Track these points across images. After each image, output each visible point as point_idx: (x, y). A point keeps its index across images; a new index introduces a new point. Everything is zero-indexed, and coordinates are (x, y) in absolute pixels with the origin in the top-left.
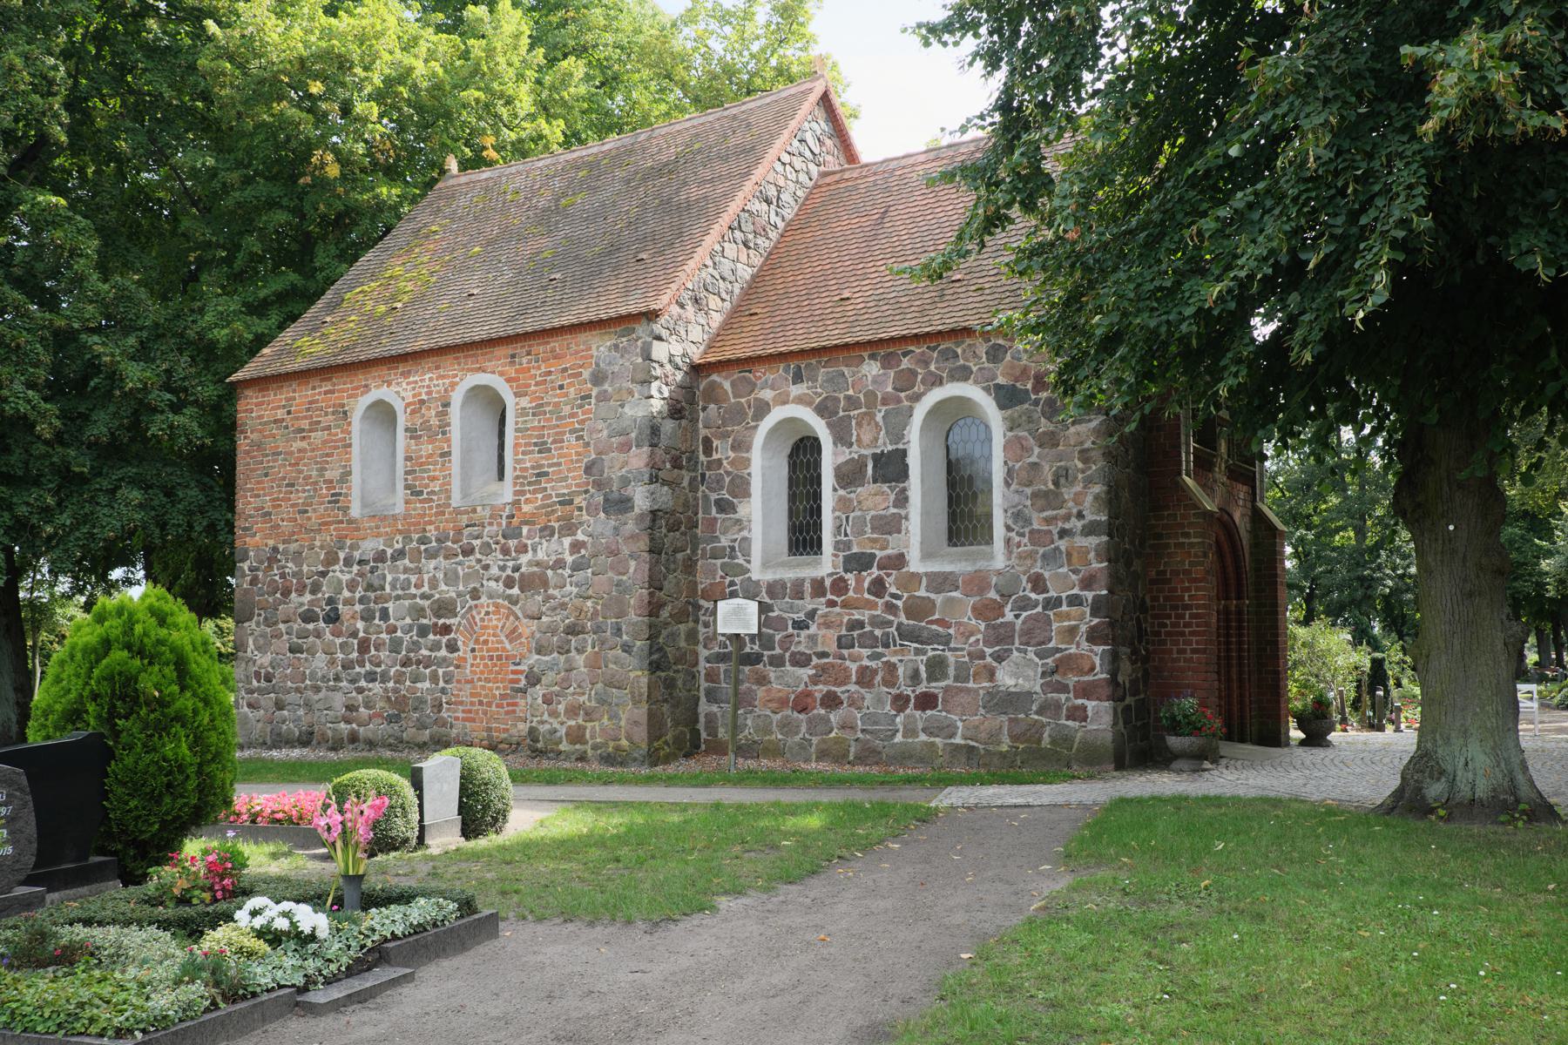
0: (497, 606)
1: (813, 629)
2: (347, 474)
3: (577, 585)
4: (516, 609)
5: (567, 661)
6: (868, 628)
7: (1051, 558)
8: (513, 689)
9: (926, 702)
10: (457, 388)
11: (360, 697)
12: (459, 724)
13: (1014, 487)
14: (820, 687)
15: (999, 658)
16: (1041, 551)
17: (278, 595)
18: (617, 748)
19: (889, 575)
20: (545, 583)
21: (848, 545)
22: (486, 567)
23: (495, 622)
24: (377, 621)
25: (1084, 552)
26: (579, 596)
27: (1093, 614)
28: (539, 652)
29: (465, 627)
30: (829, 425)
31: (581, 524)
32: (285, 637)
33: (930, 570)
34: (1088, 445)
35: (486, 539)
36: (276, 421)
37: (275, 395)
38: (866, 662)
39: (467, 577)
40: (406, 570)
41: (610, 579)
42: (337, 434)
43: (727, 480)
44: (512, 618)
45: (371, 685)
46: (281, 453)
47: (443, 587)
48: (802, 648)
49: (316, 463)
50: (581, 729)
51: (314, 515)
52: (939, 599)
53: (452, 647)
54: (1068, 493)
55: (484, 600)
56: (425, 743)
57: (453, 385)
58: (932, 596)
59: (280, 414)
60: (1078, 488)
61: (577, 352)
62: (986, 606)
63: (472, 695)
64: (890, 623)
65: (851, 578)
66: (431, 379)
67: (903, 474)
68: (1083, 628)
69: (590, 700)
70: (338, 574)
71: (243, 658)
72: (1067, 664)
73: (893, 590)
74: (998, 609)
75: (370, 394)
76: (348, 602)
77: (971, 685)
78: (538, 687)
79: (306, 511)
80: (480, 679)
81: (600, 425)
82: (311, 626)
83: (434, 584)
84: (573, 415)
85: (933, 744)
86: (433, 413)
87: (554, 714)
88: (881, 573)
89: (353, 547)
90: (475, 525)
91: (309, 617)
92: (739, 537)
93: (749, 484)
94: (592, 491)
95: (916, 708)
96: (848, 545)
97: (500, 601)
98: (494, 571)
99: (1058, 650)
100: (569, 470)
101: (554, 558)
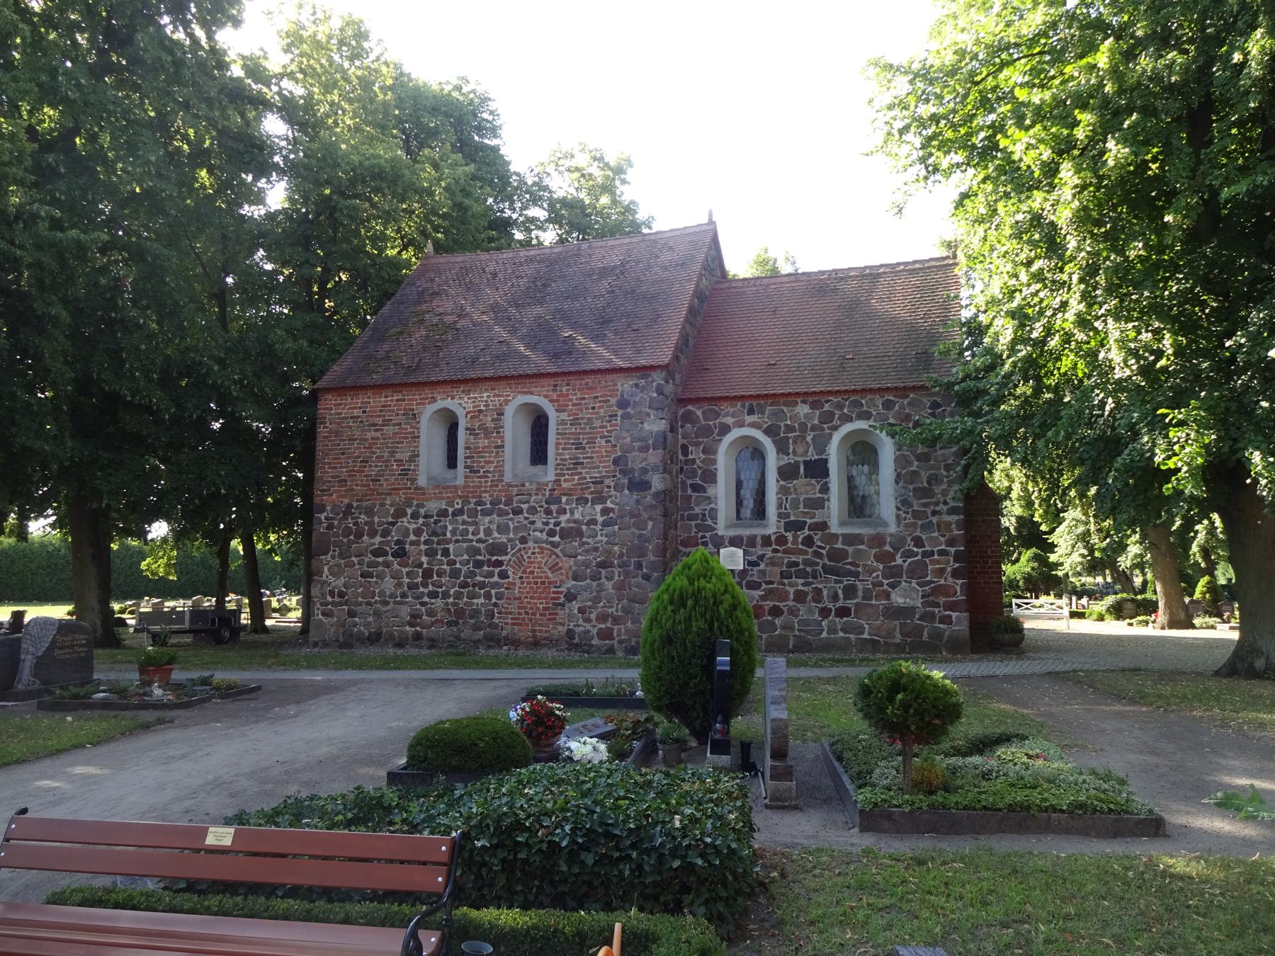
1: (762, 566)
2: (414, 457)
3: (606, 536)
4: (557, 551)
5: (599, 585)
7: (927, 527)
8: (553, 604)
9: (843, 612)
10: (510, 404)
11: (423, 609)
12: (509, 627)
13: (901, 485)
15: (893, 586)
16: (920, 523)
17: (352, 537)
19: (816, 534)
20: (580, 534)
21: (788, 515)
22: (533, 523)
23: (539, 559)
24: (439, 557)
27: (954, 561)
28: (575, 579)
29: (514, 562)
30: (774, 442)
31: (610, 497)
32: (357, 567)
33: (845, 532)
34: (950, 461)
35: (532, 504)
36: (352, 418)
37: (352, 399)
38: (800, 588)
39: (516, 529)
40: (464, 523)
43: (700, 472)
44: (554, 556)
45: (433, 601)
46: (356, 439)
47: (496, 535)
48: (755, 578)
49: (388, 447)
50: (610, 631)
51: (385, 484)
52: (850, 549)
53: (503, 575)
55: (530, 544)
57: (507, 402)
58: (846, 547)
59: (356, 412)
61: (606, 387)
63: (519, 608)
64: (818, 564)
65: (789, 536)
66: (488, 397)
67: (826, 473)
68: (949, 569)
69: (617, 611)
70: (405, 524)
71: (318, 581)
72: (938, 590)
73: (819, 543)
75: (554, 412)
76: (412, 543)
77: (873, 602)
79: (379, 480)
80: (526, 597)
82: (380, 560)
83: (488, 532)
84: (602, 427)
87: (588, 620)
89: (420, 506)
90: (523, 494)
91: (379, 552)
92: (708, 508)
93: (716, 475)
94: (619, 476)
95: (836, 616)
96: (788, 515)
97: (544, 545)
99: (932, 582)
100: (600, 462)
101: (588, 518)
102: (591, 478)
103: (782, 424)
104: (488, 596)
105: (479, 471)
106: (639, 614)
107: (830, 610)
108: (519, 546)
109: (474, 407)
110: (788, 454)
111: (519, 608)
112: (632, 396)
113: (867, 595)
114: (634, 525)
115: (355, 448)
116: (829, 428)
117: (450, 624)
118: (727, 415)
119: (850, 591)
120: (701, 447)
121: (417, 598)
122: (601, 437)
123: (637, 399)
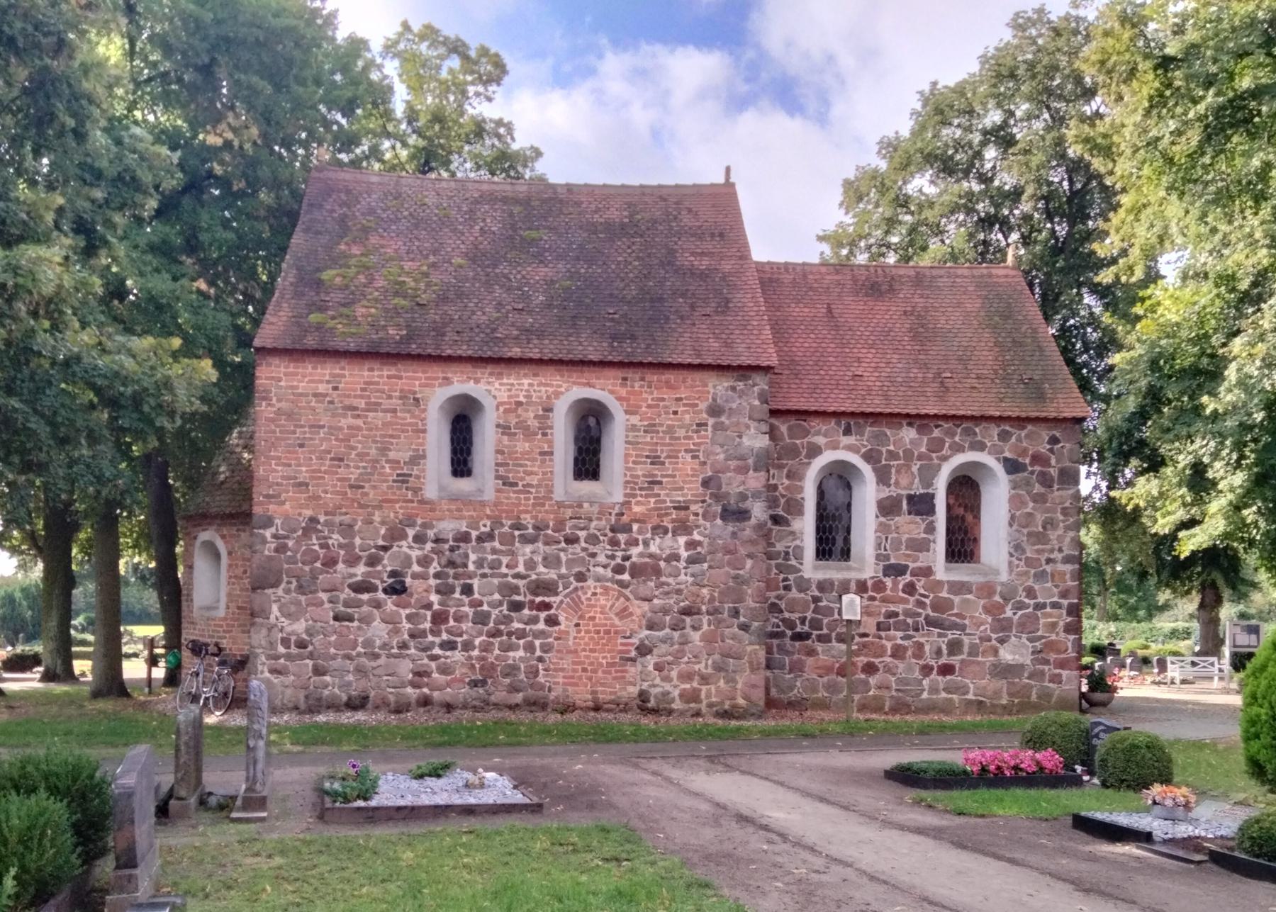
0: (606, 589)
3: (693, 575)
4: (627, 592)
5: (682, 636)
6: (901, 617)
7: (1041, 576)
8: (621, 658)
9: (946, 670)
10: (562, 397)
13: (1015, 527)
14: (862, 658)
15: (1002, 641)
16: (1033, 571)
17: (318, 565)
18: (734, 706)
20: (658, 572)
21: (887, 558)
22: (594, 555)
23: (603, 602)
24: (457, 595)
25: (1063, 574)
26: (694, 584)
29: (568, 604)
30: (875, 470)
31: (698, 527)
32: (327, 605)
33: (952, 579)
34: (1067, 504)
35: (592, 531)
36: (315, 395)
38: (899, 642)
39: (570, 563)
40: (494, 551)
41: (728, 573)
42: (405, 419)
43: (783, 501)
45: (448, 653)
46: (323, 427)
47: (541, 569)
53: (552, 621)
54: (1053, 535)
55: (590, 582)
56: (517, 705)
57: (557, 395)
59: (322, 388)
60: (1060, 532)
61: (692, 387)
62: (993, 606)
63: (574, 663)
64: (919, 615)
65: (888, 582)
66: (530, 385)
67: (931, 510)
68: (1061, 623)
69: (707, 667)
70: (405, 549)
71: (262, 625)
72: (1050, 646)
73: (922, 591)
74: (1001, 609)
75: (623, 413)
76: (415, 576)
77: (980, 659)
78: (649, 657)
79: (362, 487)
80: (584, 650)
81: (718, 450)
82: (365, 597)
84: (686, 438)
85: (951, 700)
86: (532, 415)
87: (667, 679)
88: (914, 579)
90: (580, 518)
91: (359, 588)
92: (793, 545)
93: (802, 506)
94: (709, 501)
96: (887, 558)
97: (609, 584)
98: (601, 559)
99: (1043, 637)
101: (668, 552)
102: (672, 502)
103: (884, 450)
104: (530, 648)
105: (516, 484)
106: (734, 672)
107: (932, 668)
108: (575, 584)
109: (509, 397)
110: (889, 486)
111: (574, 663)
112: (727, 401)
113: (973, 651)
114: (729, 564)
115: (322, 440)
116: (938, 458)
117: (474, 684)
118: (818, 433)
119: (955, 647)
120: (785, 471)
121: (424, 650)
122: (686, 451)
123: (734, 406)
